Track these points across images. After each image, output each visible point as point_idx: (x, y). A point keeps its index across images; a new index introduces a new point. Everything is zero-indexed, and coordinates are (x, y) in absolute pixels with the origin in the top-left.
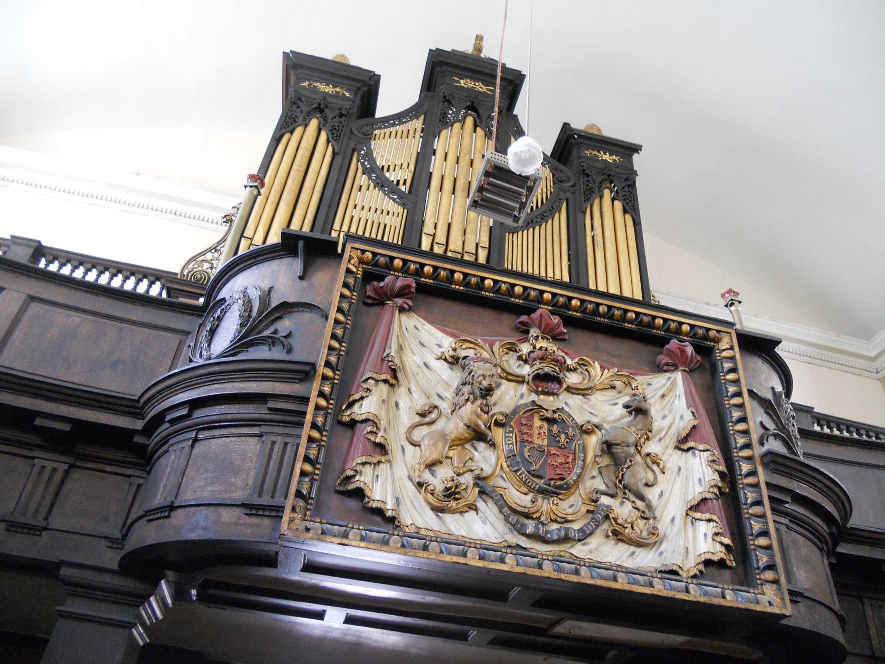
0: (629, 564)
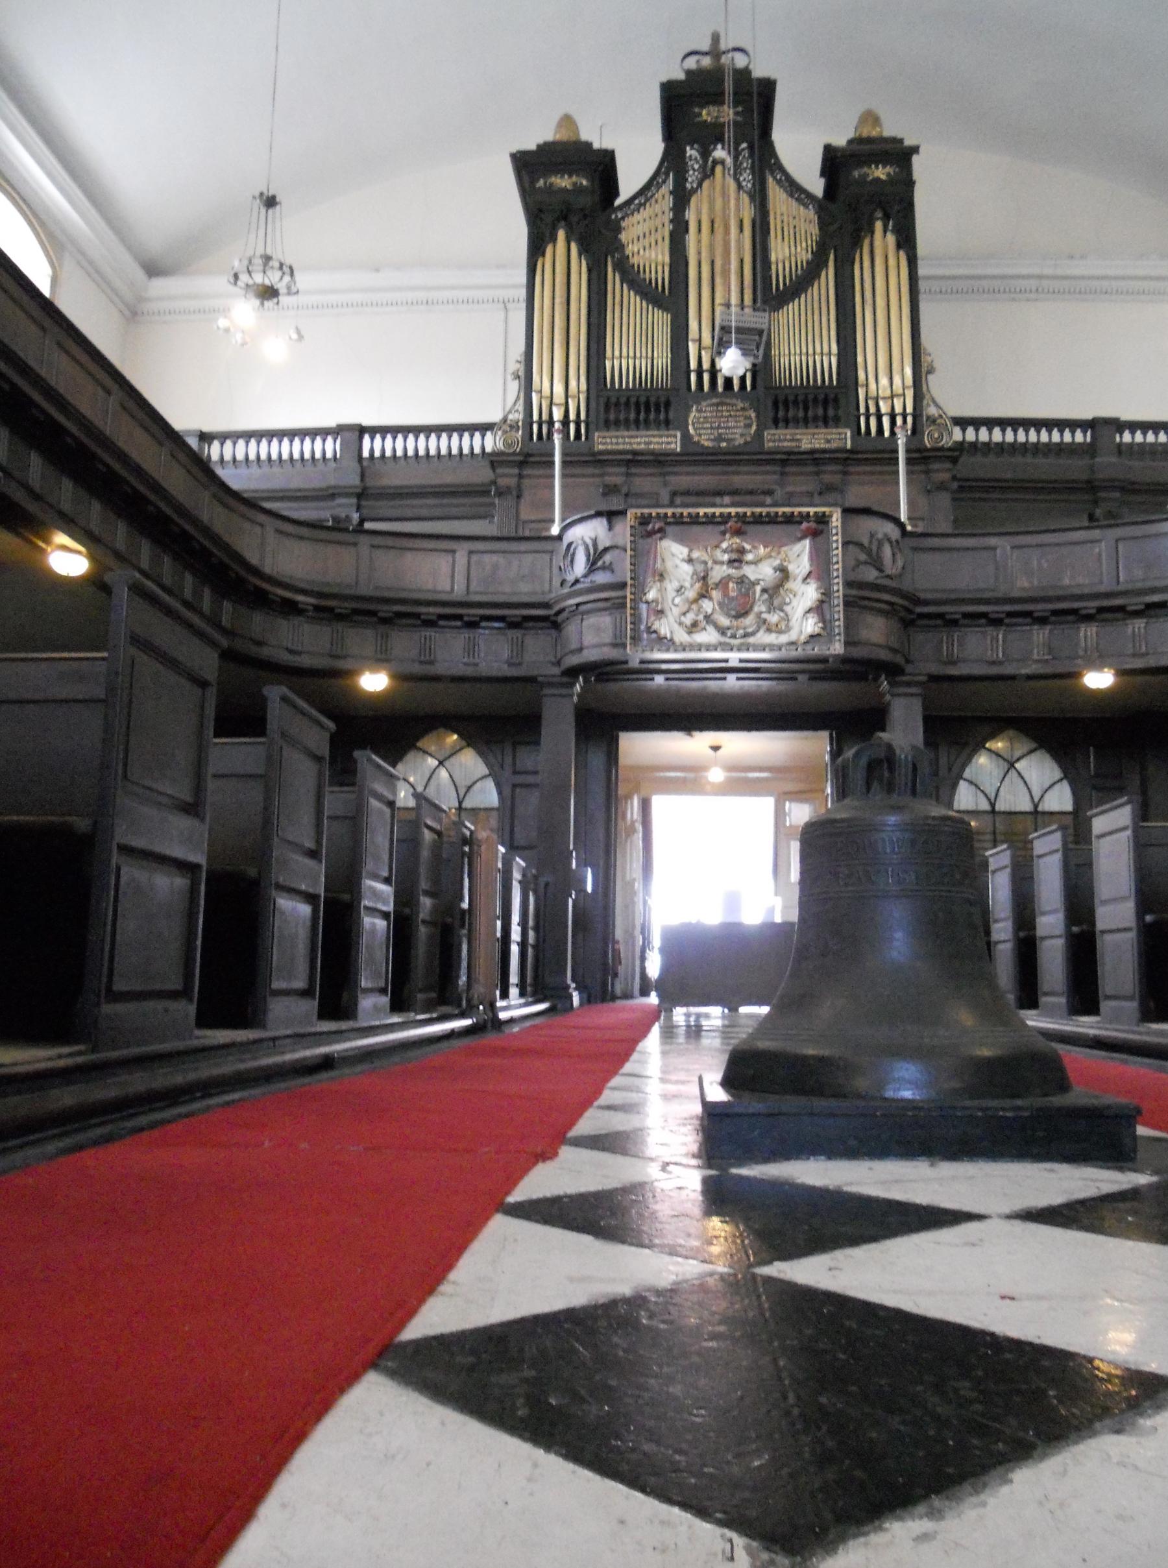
0: (775, 642)
